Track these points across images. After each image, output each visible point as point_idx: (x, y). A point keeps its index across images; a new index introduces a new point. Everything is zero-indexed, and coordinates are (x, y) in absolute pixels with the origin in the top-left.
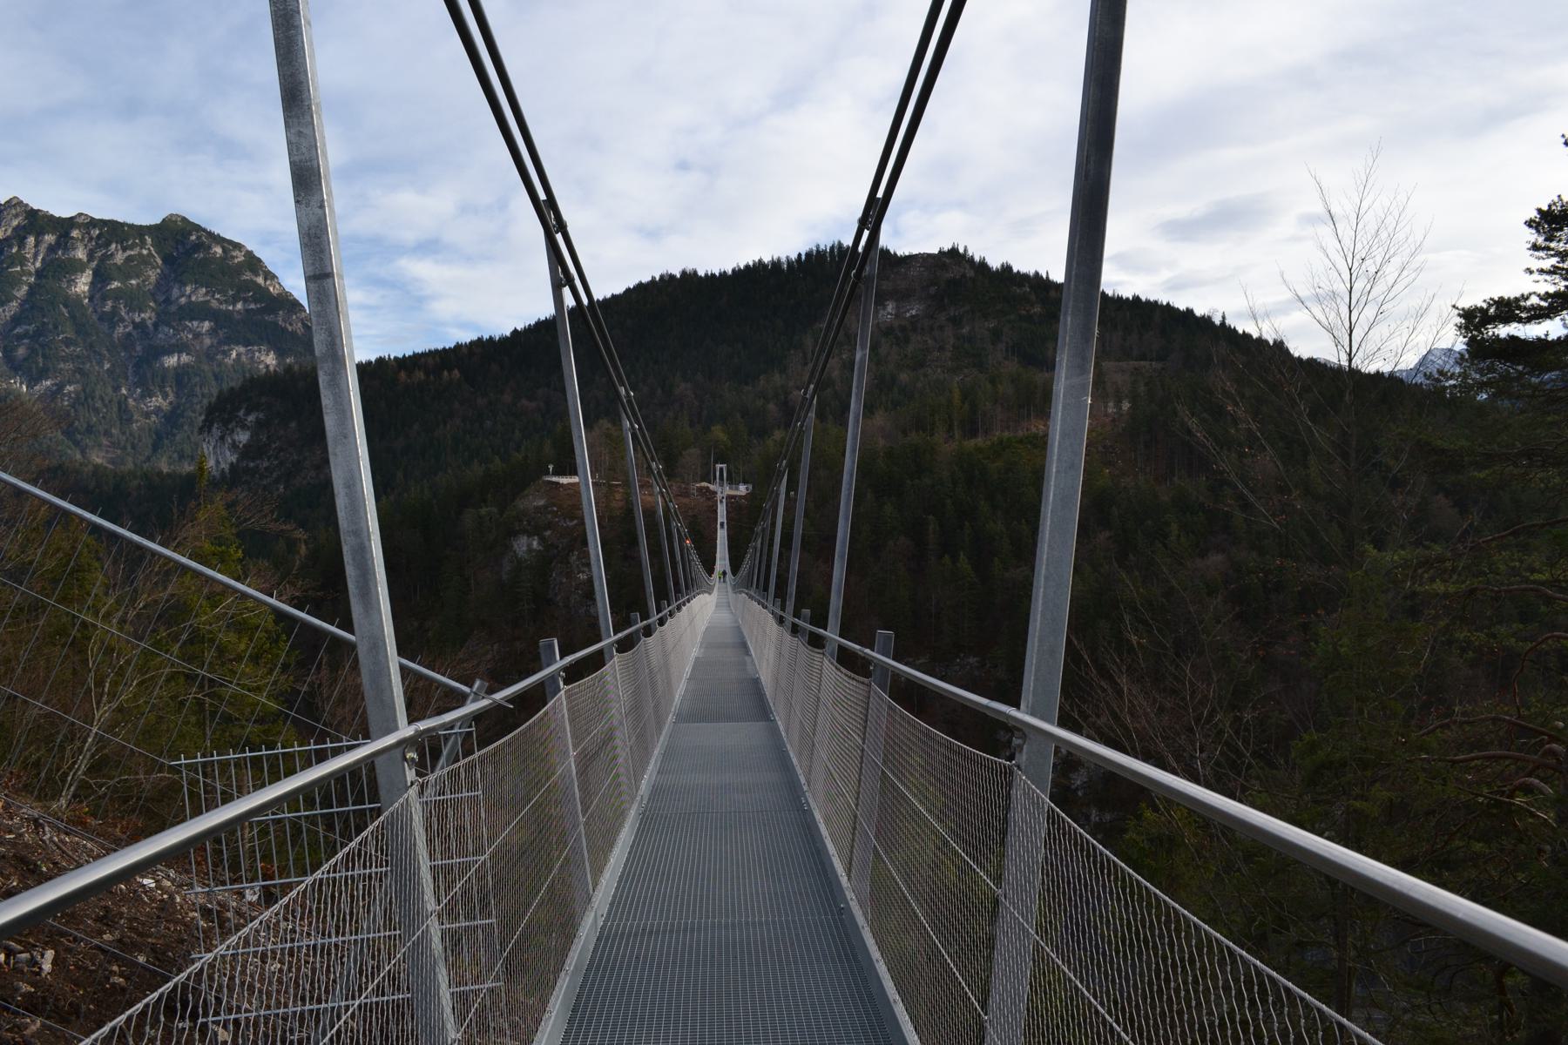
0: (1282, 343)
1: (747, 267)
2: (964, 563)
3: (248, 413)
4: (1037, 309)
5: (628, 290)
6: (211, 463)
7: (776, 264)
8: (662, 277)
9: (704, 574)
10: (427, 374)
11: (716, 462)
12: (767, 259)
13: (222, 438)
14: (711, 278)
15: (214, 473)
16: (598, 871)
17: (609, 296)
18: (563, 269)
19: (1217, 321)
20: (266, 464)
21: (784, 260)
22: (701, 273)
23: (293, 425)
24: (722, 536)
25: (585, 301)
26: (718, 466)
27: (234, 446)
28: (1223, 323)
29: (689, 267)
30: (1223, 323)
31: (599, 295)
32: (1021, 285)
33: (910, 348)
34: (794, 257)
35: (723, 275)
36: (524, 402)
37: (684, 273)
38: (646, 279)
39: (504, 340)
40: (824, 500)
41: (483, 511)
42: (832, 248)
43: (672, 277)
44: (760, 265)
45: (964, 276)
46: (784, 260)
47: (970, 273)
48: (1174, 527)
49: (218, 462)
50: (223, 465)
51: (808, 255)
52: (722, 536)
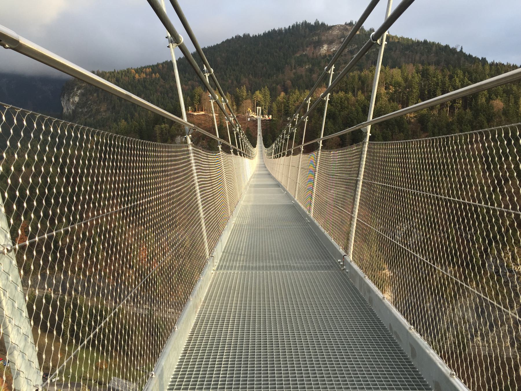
0: (485, 59)
1: (269, 32)
3: (77, 90)
5: (223, 42)
6: (65, 110)
7: (280, 31)
8: (236, 36)
9: (249, 146)
10: (146, 75)
11: (257, 106)
12: (277, 29)
13: (69, 100)
14: (255, 37)
15: (67, 114)
16: (214, 241)
17: (215, 44)
19: (458, 50)
20: (86, 110)
21: (283, 29)
22: (242, 35)
23: (95, 95)
24: (259, 132)
25: (191, 49)
26: (258, 108)
28: (461, 51)
29: (247, 33)
30: (461, 51)
34: (287, 27)
37: (244, 35)
41: (163, 126)
42: (302, 24)
43: (240, 37)
46: (283, 29)
49: (68, 109)
50: (70, 111)
51: (293, 26)
52: (259, 132)
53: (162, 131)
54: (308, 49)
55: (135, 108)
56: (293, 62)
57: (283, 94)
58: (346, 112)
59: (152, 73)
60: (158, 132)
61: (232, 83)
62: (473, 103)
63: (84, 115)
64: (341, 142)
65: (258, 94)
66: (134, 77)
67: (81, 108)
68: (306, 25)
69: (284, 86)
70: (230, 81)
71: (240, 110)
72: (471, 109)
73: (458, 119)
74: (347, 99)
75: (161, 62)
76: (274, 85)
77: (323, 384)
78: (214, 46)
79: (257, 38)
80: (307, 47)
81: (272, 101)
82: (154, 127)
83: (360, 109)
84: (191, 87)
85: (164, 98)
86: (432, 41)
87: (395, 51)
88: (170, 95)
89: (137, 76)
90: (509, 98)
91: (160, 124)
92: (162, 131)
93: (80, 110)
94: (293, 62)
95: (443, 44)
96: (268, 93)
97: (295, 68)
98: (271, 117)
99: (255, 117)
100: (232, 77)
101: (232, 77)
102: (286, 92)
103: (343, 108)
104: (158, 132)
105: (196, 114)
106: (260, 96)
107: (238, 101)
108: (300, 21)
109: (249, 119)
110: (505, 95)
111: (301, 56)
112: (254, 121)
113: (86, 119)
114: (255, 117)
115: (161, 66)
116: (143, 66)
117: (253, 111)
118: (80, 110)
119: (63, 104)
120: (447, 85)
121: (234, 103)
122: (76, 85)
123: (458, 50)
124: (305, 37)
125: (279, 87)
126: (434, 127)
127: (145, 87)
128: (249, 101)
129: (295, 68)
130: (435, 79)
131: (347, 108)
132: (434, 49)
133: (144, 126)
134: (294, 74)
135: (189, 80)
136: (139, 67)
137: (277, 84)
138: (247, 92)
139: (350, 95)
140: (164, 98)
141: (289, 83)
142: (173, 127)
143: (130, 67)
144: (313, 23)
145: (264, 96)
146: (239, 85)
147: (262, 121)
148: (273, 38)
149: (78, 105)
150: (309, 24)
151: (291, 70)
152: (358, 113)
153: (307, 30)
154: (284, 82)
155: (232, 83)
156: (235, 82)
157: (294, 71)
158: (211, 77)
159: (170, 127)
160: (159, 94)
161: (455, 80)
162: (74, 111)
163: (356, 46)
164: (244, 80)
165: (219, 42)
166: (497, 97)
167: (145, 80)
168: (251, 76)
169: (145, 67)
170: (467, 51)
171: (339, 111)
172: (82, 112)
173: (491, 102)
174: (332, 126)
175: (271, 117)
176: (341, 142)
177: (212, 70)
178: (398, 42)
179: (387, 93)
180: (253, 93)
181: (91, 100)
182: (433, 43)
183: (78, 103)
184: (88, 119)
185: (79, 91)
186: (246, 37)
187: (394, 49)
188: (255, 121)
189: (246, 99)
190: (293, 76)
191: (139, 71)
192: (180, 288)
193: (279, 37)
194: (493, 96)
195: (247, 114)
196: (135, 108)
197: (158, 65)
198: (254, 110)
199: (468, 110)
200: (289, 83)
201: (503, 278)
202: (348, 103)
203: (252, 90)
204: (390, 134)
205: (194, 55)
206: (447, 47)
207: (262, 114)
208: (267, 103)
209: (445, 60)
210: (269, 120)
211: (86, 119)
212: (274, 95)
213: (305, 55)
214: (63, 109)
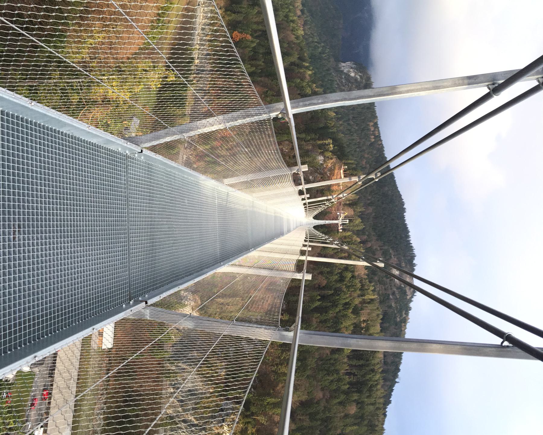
1: (407, 228)
2: (318, 304)
3: (359, 75)
4: (398, 319)
6: (343, 64)
7: (408, 237)
9: (316, 213)
10: (373, 131)
12: (410, 234)
13: (352, 68)
14: (403, 217)
18: (422, 345)
19: (397, 380)
22: (405, 214)
26: (348, 220)
27: (349, 71)
28: (396, 382)
29: (407, 210)
30: (396, 382)
31: (396, 172)
32: (405, 314)
33: (385, 279)
34: (411, 242)
35: (405, 221)
36: (365, 161)
37: (405, 209)
38: (403, 197)
39: (384, 154)
40: (336, 254)
41: (331, 146)
43: (404, 205)
44: (408, 232)
45: (407, 295)
47: (408, 297)
48: (332, 378)
52: (327, 222)
53: (327, 145)
54: (396, 259)
55: (347, 121)
56: (386, 247)
57: (359, 240)
58: (345, 290)
59: (374, 135)
60: (327, 142)
61: (368, 200)
62: (353, 390)
63: (339, 80)
64: (321, 286)
65: (359, 220)
66: (371, 121)
67: (345, 77)
68: (413, 257)
69: (367, 241)
70: (370, 198)
71: (346, 207)
72: (348, 388)
73: (341, 379)
74: (355, 291)
75: (383, 143)
76: (367, 233)
77: (78, 288)
78: (396, 185)
79: (402, 218)
80: (397, 258)
81: (353, 231)
82: (331, 138)
83: (347, 301)
84: (364, 166)
85: (355, 144)
86: (403, 357)
87: (395, 328)
88: (358, 150)
89: (372, 124)
90: (358, 419)
91: (333, 144)
92: (327, 145)
93: (343, 77)
94: (386, 247)
95: (401, 367)
96: (360, 228)
97: (381, 249)
98: (341, 231)
99: (341, 218)
100: (373, 199)
101: (373, 199)
102: (360, 243)
103: (348, 287)
104: (327, 142)
105: (342, 171)
106: (357, 222)
107: (351, 204)
108: (416, 252)
109: (338, 214)
110: (360, 415)
111: (390, 254)
112: (337, 217)
113: (336, 81)
114: (341, 218)
115: (380, 143)
116: (380, 129)
117: (345, 217)
118: (343, 77)
119: (348, 63)
120: (367, 368)
121: (351, 202)
122: (364, 75)
123: (397, 380)
124: (404, 256)
125: (366, 237)
126: (335, 360)
127: (363, 130)
128: (352, 213)
129: (381, 249)
130: (371, 358)
131: (348, 291)
132: (398, 360)
133: (331, 131)
134: (376, 249)
135: (370, 165)
136: (379, 126)
137: (368, 236)
138: (360, 212)
139: (359, 292)
140: (355, 144)
141: (369, 245)
142: (331, 154)
143: (379, 118)
144: (414, 262)
145: (357, 225)
146: (367, 205)
147: (337, 224)
148: (403, 231)
149: (347, 75)
150: (414, 259)
151: (379, 246)
152: (344, 299)
153: (409, 258)
154: (370, 241)
155: (368, 200)
156: (369, 202)
157: (379, 248)
158: (373, 179)
159: (331, 151)
160: (358, 141)
161: (371, 374)
162: (342, 71)
163: (398, 297)
164: (370, 210)
165: (399, 189)
166: (359, 408)
167: (369, 130)
168: (373, 214)
169: (379, 131)
170: (396, 388)
171: (346, 285)
172: (342, 78)
173: (355, 404)
174: (334, 280)
175: (341, 231)
176: (321, 286)
177: (377, 180)
178: (402, 331)
179: (360, 322)
180: (359, 216)
181: (352, 86)
182: (401, 359)
183: (349, 75)
184: (336, 83)
185: (359, 77)
186: (404, 210)
187: (397, 327)
188: (337, 219)
189: (354, 211)
190: (375, 247)
191: (376, 125)
192: (202, 164)
193: (403, 236)
194: (359, 405)
195: (342, 212)
196: (347, 121)
197: (381, 141)
198: (345, 218)
199: (348, 386)
200: (369, 245)
201: (219, 414)
202: (352, 291)
203: (361, 216)
204: (329, 325)
205: (389, 166)
206: (399, 370)
207: (343, 224)
208: (351, 228)
209: (388, 369)
210: (338, 230)
211: (336, 81)
212: (358, 233)
213: (391, 257)
214: (344, 62)
